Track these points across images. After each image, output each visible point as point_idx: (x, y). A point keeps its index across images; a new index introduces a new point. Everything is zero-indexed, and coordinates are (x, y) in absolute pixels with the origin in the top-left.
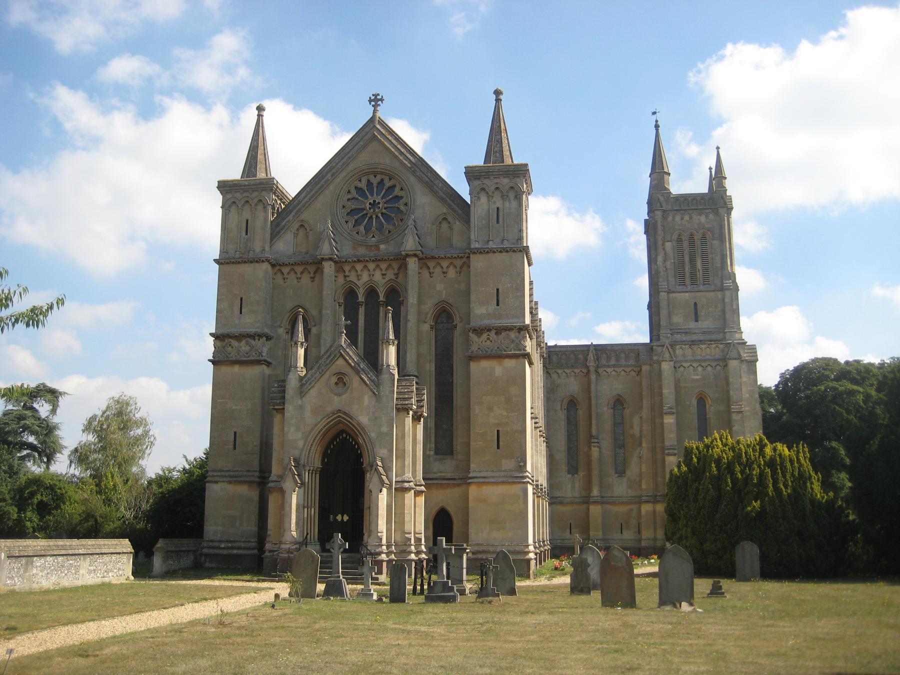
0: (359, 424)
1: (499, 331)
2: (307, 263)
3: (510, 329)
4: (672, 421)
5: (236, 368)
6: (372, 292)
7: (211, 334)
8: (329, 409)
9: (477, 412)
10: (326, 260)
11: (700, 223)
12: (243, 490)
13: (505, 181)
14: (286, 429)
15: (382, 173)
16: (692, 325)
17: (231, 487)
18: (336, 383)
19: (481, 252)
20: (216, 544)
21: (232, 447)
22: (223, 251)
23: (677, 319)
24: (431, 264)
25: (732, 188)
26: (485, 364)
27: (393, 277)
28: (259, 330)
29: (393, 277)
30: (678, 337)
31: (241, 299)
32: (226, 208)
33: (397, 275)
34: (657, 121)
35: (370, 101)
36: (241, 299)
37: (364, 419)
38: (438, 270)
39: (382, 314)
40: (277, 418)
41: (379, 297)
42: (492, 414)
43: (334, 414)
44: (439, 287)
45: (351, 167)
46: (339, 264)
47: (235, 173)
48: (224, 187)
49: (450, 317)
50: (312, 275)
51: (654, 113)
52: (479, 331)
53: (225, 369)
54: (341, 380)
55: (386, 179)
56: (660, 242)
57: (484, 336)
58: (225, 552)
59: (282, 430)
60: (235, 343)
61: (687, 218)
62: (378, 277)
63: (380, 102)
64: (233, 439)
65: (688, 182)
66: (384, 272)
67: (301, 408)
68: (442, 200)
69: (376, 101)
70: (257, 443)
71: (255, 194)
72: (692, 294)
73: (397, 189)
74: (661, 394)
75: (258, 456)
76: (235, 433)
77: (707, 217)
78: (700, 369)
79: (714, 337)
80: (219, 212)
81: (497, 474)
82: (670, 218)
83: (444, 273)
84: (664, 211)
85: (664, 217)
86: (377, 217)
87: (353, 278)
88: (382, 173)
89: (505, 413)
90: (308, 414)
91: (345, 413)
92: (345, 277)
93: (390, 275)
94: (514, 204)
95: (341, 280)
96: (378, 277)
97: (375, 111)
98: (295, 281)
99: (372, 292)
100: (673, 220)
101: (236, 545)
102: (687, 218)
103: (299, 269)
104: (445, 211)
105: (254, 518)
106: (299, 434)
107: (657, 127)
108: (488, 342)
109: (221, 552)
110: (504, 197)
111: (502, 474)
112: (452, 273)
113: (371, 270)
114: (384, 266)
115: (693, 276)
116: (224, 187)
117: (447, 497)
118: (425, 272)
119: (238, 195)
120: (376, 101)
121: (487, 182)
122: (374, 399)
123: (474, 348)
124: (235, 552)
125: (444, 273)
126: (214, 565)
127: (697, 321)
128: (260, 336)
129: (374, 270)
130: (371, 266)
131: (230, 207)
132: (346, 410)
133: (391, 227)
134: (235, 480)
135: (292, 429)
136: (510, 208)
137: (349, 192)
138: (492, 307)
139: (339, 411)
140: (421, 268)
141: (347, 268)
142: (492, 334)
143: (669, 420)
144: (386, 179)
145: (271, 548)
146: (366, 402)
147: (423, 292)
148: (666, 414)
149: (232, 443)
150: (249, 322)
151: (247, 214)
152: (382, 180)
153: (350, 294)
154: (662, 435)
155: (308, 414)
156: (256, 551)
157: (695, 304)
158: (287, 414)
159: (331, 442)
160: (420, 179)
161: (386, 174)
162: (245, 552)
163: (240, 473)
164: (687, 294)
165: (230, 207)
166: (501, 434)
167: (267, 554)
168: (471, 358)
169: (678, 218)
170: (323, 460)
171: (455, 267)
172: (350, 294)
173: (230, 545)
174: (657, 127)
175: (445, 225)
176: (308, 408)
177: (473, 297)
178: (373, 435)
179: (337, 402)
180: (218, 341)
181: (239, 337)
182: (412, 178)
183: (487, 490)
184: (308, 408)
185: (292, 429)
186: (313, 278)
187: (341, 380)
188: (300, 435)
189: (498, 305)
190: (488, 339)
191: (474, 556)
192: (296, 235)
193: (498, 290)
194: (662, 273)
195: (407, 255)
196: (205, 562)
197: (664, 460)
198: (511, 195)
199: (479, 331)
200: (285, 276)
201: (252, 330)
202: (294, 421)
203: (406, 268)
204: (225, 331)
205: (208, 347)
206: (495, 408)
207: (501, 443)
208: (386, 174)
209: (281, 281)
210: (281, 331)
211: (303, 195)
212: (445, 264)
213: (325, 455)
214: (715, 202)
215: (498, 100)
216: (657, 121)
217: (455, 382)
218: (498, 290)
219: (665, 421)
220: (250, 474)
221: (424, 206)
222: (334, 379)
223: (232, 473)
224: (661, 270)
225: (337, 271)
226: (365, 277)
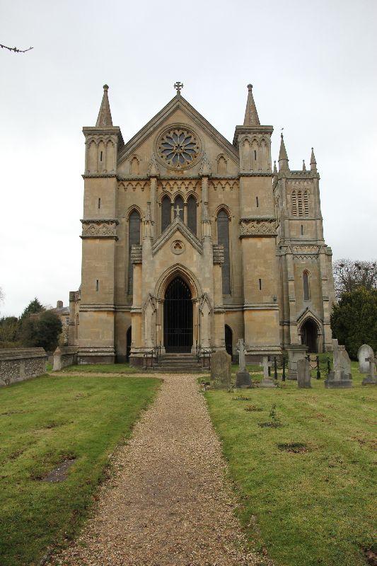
1: (259, 221)
2: (139, 180)
5: (97, 241)
6: (179, 198)
10: (153, 177)
12: (104, 316)
13: (260, 136)
14: (143, 275)
15: (182, 129)
16: (301, 236)
19: (247, 176)
20: (87, 350)
21: (95, 289)
22: (88, 170)
23: (293, 234)
24: (215, 182)
25: (320, 169)
26: (251, 240)
27: (192, 189)
28: (112, 219)
29: (192, 189)
30: (294, 243)
32: (88, 144)
33: (195, 188)
35: (175, 86)
37: (194, 270)
38: (219, 186)
39: (173, 213)
40: (136, 269)
43: (174, 266)
44: (220, 196)
45: (164, 125)
46: (159, 180)
47: (92, 122)
48: (87, 131)
52: (247, 221)
54: (178, 244)
55: (185, 133)
56: (284, 195)
57: (250, 224)
58: (93, 354)
59: (141, 276)
62: (183, 189)
66: (187, 186)
67: (153, 262)
70: (112, 286)
71: (107, 136)
73: (192, 138)
74: (287, 271)
75: (113, 295)
79: (311, 243)
80: (84, 147)
81: (261, 305)
86: (180, 155)
87: (168, 189)
88: (182, 129)
89: (264, 269)
90: (157, 266)
91: (183, 266)
92: (163, 188)
93: (191, 188)
95: (161, 190)
96: (183, 189)
97: (179, 92)
99: (179, 198)
102: (297, 183)
106: (149, 281)
107: (282, 136)
109: (90, 354)
110: (260, 146)
111: (264, 305)
112: (227, 188)
114: (187, 182)
116: (87, 131)
119: (96, 137)
120: (178, 86)
121: (249, 135)
122: (200, 257)
124: (99, 354)
126: (86, 363)
128: (112, 222)
131: (90, 143)
132: (182, 263)
133: (189, 161)
137: (163, 139)
138: (255, 207)
139: (178, 264)
141: (164, 183)
143: (291, 284)
146: (195, 259)
147: (212, 198)
149: (95, 287)
150: (107, 213)
151: (102, 147)
153: (166, 198)
154: (287, 291)
155: (157, 266)
158: (143, 266)
159: (172, 282)
161: (185, 130)
162: (106, 354)
165: (90, 143)
167: (132, 355)
168: (241, 237)
169: (293, 183)
170: (165, 296)
172: (166, 198)
173: (96, 350)
174: (282, 136)
175: (222, 161)
176: (157, 262)
177: (243, 201)
179: (176, 259)
181: (98, 223)
182: (202, 133)
184: (157, 262)
187: (178, 244)
191: (249, 353)
192: (131, 163)
198: (263, 144)
199: (247, 221)
201: (107, 219)
202: (148, 271)
203: (201, 184)
204: (87, 219)
205: (79, 229)
206: (259, 268)
213: (167, 292)
215: (250, 91)
220: (85, 310)
221: (210, 149)
222: (174, 245)
223: (96, 306)
226: (175, 189)
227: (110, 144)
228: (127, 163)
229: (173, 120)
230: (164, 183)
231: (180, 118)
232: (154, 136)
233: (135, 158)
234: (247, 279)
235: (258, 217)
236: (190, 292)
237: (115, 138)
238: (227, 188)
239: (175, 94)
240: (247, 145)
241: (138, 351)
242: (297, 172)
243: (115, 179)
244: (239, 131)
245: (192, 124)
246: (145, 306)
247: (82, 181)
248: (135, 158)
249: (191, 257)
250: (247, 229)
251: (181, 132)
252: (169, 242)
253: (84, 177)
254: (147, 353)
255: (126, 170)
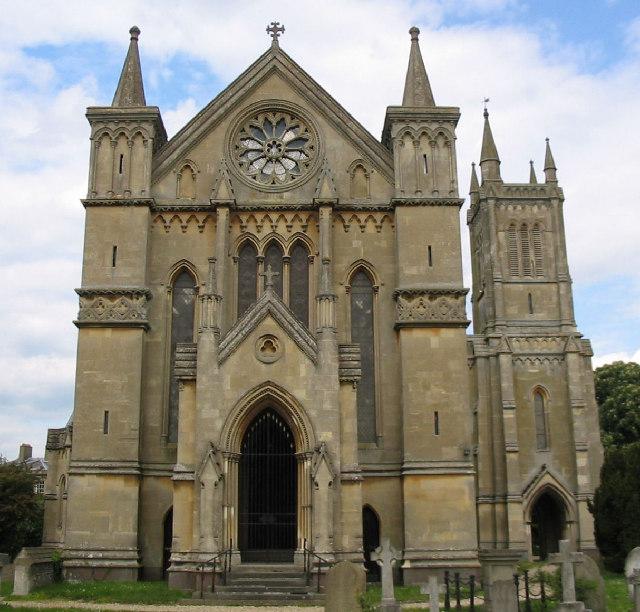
0: (294, 399)
1: (433, 294)
3: (448, 293)
4: (512, 416)
5: (108, 333)
6: (274, 245)
7: (76, 290)
8: (255, 381)
9: (411, 390)
11: (533, 214)
12: (118, 484)
14: (198, 405)
15: (282, 111)
16: (527, 316)
17: (101, 482)
18: (263, 349)
22: (93, 190)
24: (347, 217)
31: (115, 248)
32: (97, 141)
34: (486, 110)
35: (268, 30)
36: (115, 248)
37: (300, 394)
38: (354, 225)
40: (185, 393)
41: (282, 252)
42: (429, 393)
43: (261, 386)
44: (356, 243)
45: (247, 103)
49: (369, 278)
50: (201, 224)
51: (487, 101)
52: (410, 295)
53: (94, 334)
56: (493, 231)
57: (416, 301)
58: (95, 564)
60: (106, 301)
61: (519, 208)
62: (282, 229)
63: (280, 32)
64: (103, 420)
65: (514, 173)
66: (289, 223)
67: (219, 378)
68: (356, 145)
69: (275, 30)
70: (135, 424)
71: (134, 125)
72: (526, 285)
74: (499, 388)
76: (107, 412)
77: (539, 208)
78: (537, 362)
82: (503, 208)
83: (362, 227)
84: (498, 199)
85: (497, 206)
88: (282, 111)
91: (276, 386)
92: (242, 227)
93: (297, 228)
94: (443, 152)
97: (275, 41)
98: (180, 231)
99: (274, 245)
100: (506, 208)
101: (110, 554)
102: (519, 208)
103: (185, 217)
104: (360, 157)
105: (132, 521)
106: (211, 414)
107: (486, 115)
108: (421, 309)
113: (289, 220)
114: (289, 216)
115: (526, 263)
116: (95, 116)
117: (380, 494)
118: (340, 227)
119: (112, 126)
120: (275, 30)
121: (412, 125)
123: (405, 315)
125: (362, 227)
127: (531, 311)
129: (277, 221)
130: (274, 216)
134: (107, 472)
135: (207, 406)
136: (439, 157)
137: (243, 130)
138: (424, 267)
140: (334, 221)
141: (244, 218)
142: (426, 299)
143: (508, 415)
144: (288, 118)
145: (178, 559)
148: (506, 408)
150: (128, 276)
152: (283, 119)
156: (135, 563)
157: (530, 294)
160: (330, 120)
161: (288, 112)
163: (114, 464)
164: (521, 286)
166: (440, 416)
167: (172, 567)
168: (398, 328)
169: (510, 208)
171: (375, 221)
172: (248, 246)
174: (486, 115)
175: (360, 174)
176: (228, 378)
177: (402, 254)
178: (313, 413)
179: (265, 373)
180: (84, 300)
181: (112, 295)
183: (427, 485)
184: (228, 378)
185: (207, 406)
186: (203, 227)
187: (269, 342)
188: (217, 413)
189: (431, 265)
190: (421, 304)
192: (180, 177)
193: (430, 248)
194: (496, 264)
195: (322, 204)
196: (68, 577)
197: (504, 458)
198: (441, 142)
199: (410, 295)
200: (168, 224)
202: (209, 395)
204: (87, 288)
205: (72, 309)
207: (440, 427)
208: (288, 112)
209: (162, 231)
210: (162, 290)
211: (190, 130)
212: (363, 217)
213: (245, 440)
214: (546, 195)
216: (486, 110)
217: (376, 354)
218: (430, 248)
219: (505, 416)
223: (104, 464)
224: (495, 259)
225: (232, 221)
226: (267, 230)
227: (139, 141)
228: (172, 178)
229: (264, 94)
230: (244, 218)
231: (276, 91)
232: (225, 124)
233: (188, 167)
234: (411, 411)
235: (432, 286)
236: (292, 440)
237: (149, 129)
238: (370, 228)
239: (266, 43)
240: (409, 143)
241: (186, 558)
242: (518, 188)
243: (146, 210)
244: (392, 117)
245: (302, 102)
246: (202, 467)
247: (83, 210)
248: (188, 167)
249: (295, 372)
250: (411, 309)
251: (278, 116)
252: (252, 338)
253: (86, 204)
254: (203, 564)
255: (168, 192)
